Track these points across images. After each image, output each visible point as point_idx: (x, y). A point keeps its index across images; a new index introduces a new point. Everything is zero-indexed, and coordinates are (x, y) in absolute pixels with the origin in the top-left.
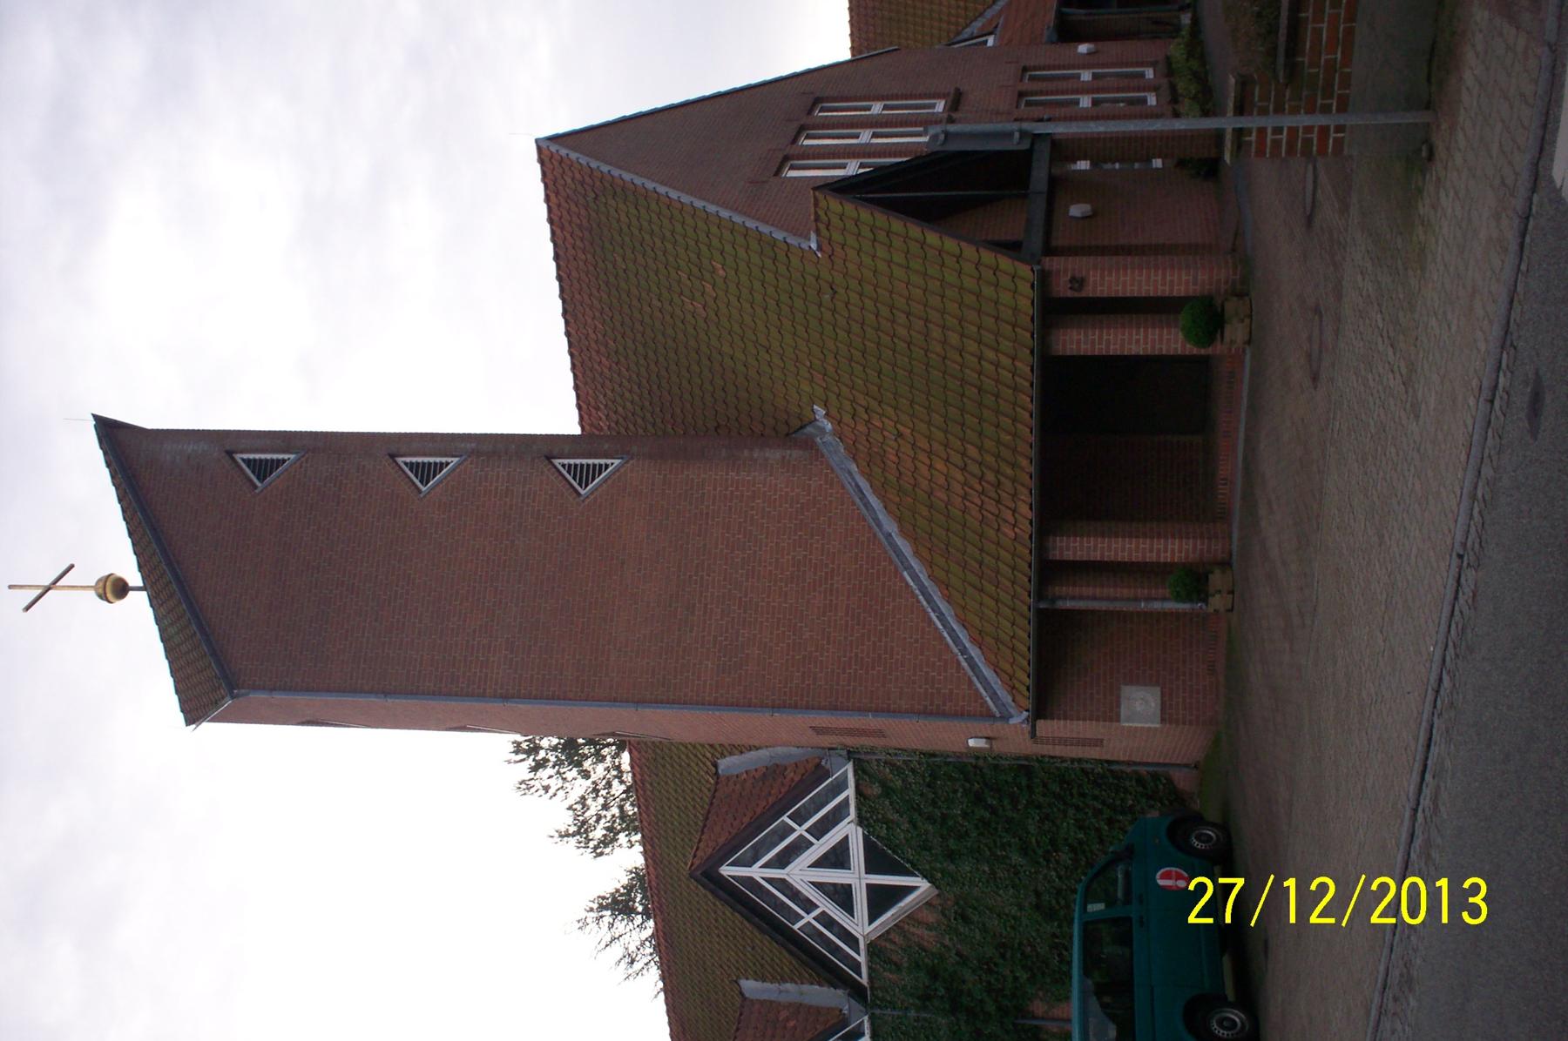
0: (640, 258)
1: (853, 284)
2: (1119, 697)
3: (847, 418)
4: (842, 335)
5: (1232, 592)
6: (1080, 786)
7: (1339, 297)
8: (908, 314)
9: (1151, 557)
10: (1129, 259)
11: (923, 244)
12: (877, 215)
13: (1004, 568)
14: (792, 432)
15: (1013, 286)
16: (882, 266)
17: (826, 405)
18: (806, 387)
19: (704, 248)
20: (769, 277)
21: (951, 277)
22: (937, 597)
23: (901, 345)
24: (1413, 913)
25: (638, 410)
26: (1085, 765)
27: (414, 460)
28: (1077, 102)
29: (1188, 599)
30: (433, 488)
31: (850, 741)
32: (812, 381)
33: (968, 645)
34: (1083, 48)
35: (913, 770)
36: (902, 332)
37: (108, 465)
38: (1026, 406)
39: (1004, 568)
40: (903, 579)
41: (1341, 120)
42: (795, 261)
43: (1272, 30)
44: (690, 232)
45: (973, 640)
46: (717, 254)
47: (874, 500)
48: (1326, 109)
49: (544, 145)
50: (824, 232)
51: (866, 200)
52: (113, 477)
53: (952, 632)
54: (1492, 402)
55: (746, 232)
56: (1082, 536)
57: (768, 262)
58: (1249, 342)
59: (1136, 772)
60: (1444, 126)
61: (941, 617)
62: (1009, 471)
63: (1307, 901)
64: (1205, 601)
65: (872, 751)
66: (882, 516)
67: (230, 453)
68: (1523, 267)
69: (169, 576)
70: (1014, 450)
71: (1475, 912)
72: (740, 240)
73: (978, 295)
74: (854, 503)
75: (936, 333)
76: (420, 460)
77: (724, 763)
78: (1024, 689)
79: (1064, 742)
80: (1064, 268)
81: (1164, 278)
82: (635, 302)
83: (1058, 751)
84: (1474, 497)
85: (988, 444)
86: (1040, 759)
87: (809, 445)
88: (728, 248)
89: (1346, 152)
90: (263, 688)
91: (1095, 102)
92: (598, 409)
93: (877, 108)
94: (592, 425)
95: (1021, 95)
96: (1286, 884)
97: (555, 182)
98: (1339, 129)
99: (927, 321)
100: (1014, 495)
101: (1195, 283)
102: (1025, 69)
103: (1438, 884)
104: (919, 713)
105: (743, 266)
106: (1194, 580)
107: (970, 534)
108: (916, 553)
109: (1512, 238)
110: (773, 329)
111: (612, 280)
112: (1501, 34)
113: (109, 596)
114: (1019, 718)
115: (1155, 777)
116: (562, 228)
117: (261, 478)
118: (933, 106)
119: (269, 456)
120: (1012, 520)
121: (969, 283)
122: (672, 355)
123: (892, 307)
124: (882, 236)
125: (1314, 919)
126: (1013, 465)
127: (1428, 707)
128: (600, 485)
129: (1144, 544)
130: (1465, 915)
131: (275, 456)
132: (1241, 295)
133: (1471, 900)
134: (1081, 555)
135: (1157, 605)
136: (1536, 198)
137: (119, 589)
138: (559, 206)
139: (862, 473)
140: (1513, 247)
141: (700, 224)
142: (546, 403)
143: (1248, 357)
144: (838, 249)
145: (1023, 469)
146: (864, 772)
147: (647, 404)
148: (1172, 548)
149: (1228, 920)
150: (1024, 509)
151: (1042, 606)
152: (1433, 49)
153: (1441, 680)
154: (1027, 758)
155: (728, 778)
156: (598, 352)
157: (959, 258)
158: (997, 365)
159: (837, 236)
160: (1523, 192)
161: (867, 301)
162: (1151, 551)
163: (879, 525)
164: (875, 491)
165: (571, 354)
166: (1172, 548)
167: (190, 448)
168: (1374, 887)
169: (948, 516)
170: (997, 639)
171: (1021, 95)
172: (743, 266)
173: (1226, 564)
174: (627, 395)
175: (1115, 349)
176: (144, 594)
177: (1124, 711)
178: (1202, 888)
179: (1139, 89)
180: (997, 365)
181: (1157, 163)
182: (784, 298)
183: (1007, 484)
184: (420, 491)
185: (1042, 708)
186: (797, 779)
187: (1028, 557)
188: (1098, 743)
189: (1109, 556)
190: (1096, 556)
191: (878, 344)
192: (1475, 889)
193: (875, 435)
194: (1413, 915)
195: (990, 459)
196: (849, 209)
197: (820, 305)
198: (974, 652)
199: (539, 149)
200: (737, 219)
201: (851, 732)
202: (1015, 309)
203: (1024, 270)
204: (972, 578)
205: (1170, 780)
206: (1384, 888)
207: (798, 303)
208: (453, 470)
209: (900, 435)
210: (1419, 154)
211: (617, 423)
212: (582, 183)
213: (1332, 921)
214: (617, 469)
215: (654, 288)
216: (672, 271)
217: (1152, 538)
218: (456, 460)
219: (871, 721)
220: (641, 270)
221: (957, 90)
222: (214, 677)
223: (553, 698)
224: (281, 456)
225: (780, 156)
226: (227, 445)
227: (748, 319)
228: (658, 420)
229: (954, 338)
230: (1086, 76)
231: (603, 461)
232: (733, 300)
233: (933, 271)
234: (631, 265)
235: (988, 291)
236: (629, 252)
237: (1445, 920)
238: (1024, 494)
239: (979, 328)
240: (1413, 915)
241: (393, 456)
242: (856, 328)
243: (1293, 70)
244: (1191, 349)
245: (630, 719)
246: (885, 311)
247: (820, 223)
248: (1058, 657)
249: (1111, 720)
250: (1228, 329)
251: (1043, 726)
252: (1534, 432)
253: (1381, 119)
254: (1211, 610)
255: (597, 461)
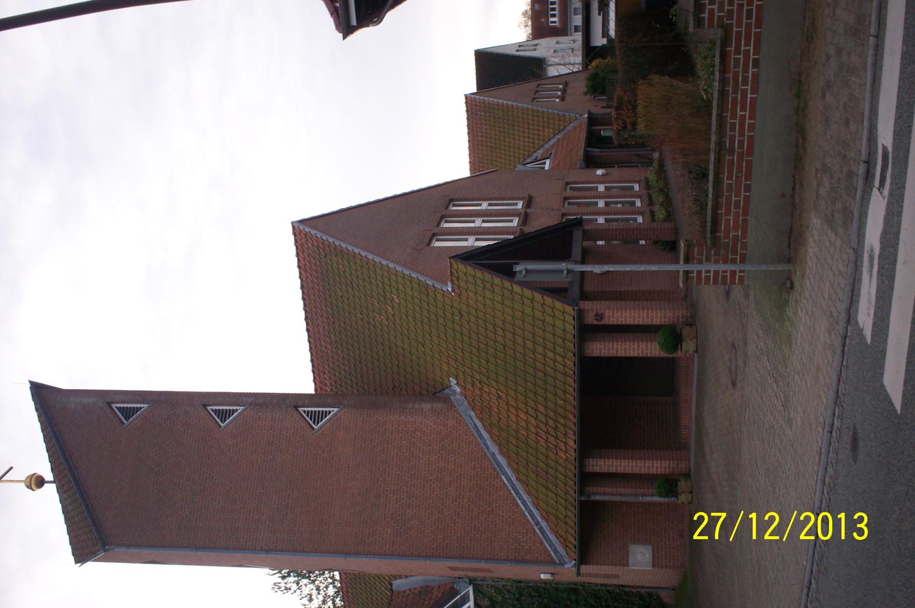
0: (350, 290)
1: (472, 311)
2: (628, 552)
3: (469, 386)
4: (466, 339)
5: (691, 493)
6: (606, 601)
7: (746, 344)
8: (503, 330)
9: (644, 471)
10: (628, 303)
11: (512, 292)
12: (485, 274)
13: (560, 476)
14: (436, 393)
15: (562, 317)
16: (489, 302)
17: (456, 379)
18: (445, 367)
19: (387, 287)
20: (424, 305)
21: (528, 311)
22: (521, 492)
23: (500, 347)
24: (825, 533)
25: (348, 375)
26: (609, 588)
27: (217, 408)
28: (596, 203)
29: (667, 495)
30: (228, 425)
31: (470, 574)
32: (448, 364)
33: (540, 520)
34: (599, 172)
35: (508, 591)
36: (500, 339)
37: (37, 410)
38: (572, 384)
39: (560, 476)
40: (501, 480)
41: (742, 267)
42: (439, 297)
43: (703, 208)
44: (379, 277)
45: (543, 517)
46: (394, 290)
47: (485, 435)
48: (734, 261)
49: (296, 225)
50: (456, 282)
51: (479, 264)
52: (39, 417)
53: (530, 512)
54: (831, 432)
55: (411, 280)
56: (605, 458)
57: (424, 297)
58: (696, 351)
59: (639, 592)
60: (798, 273)
61: (524, 503)
62: (562, 421)
63: (763, 527)
64: (676, 496)
65: (484, 579)
66: (489, 443)
67: (109, 404)
68: (844, 363)
69: (70, 477)
70: (565, 409)
71: (861, 532)
72: (408, 283)
73: (543, 321)
74: (473, 435)
75: (519, 340)
76: (221, 408)
77: (396, 583)
78: (572, 547)
79: (597, 576)
80: (591, 308)
81: (648, 314)
82: (347, 315)
83: (594, 580)
84: (824, 482)
85: (550, 404)
86: (583, 585)
87: (447, 400)
88: (401, 287)
89: (745, 283)
90: (123, 545)
91: (607, 204)
92: (324, 373)
93: (485, 205)
94: (321, 388)
95: (565, 199)
96: (750, 516)
97: (302, 246)
98: (741, 271)
99: (514, 334)
100: (565, 435)
101: (665, 317)
102: (567, 184)
103: (839, 516)
104: (511, 561)
105: (409, 298)
106: (669, 485)
107: (540, 456)
108: (509, 465)
109: (837, 344)
110: (426, 334)
111: (334, 301)
112: (827, 235)
113: (33, 486)
114: (570, 565)
115: (650, 595)
116: (306, 271)
117: (127, 418)
118: (516, 204)
119: (132, 405)
120: (564, 448)
121: (538, 314)
122: (368, 351)
123: (494, 325)
124: (488, 286)
125: (767, 537)
126: (565, 418)
127: (804, 597)
128: (326, 423)
129: (641, 463)
130: (855, 534)
131: (135, 405)
132: (691, 325)
133: (859, 526)
134: (604, 470)
135: (649, 499)
136: (849, 328)
137: (38, 482)
138: (304, 259)
139: (478, 418)
140: (839, 351)
141: (385, 273)
142: (295, 376)
143: (696, 359)
144: (464, 292)
145: (570, 420)
146: (479, 591)
147: (353, 372)
148: (656, 466)
149: (717, 537)
150: (571, 443)
151: (583, 498)
152: (790, 232)
153: (810, 582)
154: (575, 584)
155: (399, 593)
156: (325, 341)
157: (532, 300)
158: (554, 361)
159: (462, 284)
160: (842, 324)
161: (480, 321)
162: (644, 467)
163: (488, 448)
164: (485, 428)
165: (309, 342)
166: (656, 466)
167: (86, 400)
168: (802, 518)
169: (528, 444)
170: (557, 517)
171: (565, 199)
172: (409, 298)
173: (687, 476)
174: (342, 366)
175: (621, 353)
176: (54, 485)
177: (631, 560)
178: (701, 519)
179: (632, 213)
180: (554, 361)
181: (642, 242)
182: (433, 317)
183: (562, 429)
184: (220, 426)
185: (583, 559)
186: (440, 595)
187: (574, 471)
188: (617, 576)
189: (620, 470)
190: (613, 470)
191: (486, 329)
192: (861, 519)
193: (485, 396)
194: (825, 534)
195: (551, 414)
196: (470, 270)
197: (453, 322)
198: (544, 524)
199: (293, 227)
200: (406, 272)
201: (471, 570)
202: (564, 330)
203: (569, 309)
204: (541, 481)
205: (659, 597)
206: (808, 519)
207: (441, 320)
208: (240, 414)
209: (499, 397)
210: (786, 285)
211: (335, 382)
212: (318, 247)
213: (777, 538)
214: (336, 414)
215: (358, 307)
216: (369, 299)
217: (645, 459)
218: (242, 408)
219: (483, 565)
220: (351, 297)
221: (530, 195)
222: (93, 536)
223: (295, 551)
224: (139, 406)
225: (430, 234)
226: (107, 399)
227: (412, 328)
228: (360, 382)
229: (530, 345)
230: (601, 188)
231: (328, 409)
232: (404, 316)
233: (518, 306)
234: (345, 293)
235: (549, 320)
236: (344, 287)
237: (843, 537)
238: (571, 434)
239: (544, 339)
240: (825, 534)
241: (205, 406)
242: (474, 335)
243: (715, 240)
244: (663, 354)
245: (340, 560)
246: (490, 327)
247: (454, 277)
248: (592, 527)
249: (624, 565)
250: (684, 344)
251: (584, 569)
252: (855, 461)
253: (764, 268)
254: (680, 502)
255: (324, 409)
